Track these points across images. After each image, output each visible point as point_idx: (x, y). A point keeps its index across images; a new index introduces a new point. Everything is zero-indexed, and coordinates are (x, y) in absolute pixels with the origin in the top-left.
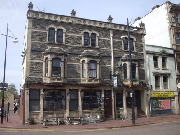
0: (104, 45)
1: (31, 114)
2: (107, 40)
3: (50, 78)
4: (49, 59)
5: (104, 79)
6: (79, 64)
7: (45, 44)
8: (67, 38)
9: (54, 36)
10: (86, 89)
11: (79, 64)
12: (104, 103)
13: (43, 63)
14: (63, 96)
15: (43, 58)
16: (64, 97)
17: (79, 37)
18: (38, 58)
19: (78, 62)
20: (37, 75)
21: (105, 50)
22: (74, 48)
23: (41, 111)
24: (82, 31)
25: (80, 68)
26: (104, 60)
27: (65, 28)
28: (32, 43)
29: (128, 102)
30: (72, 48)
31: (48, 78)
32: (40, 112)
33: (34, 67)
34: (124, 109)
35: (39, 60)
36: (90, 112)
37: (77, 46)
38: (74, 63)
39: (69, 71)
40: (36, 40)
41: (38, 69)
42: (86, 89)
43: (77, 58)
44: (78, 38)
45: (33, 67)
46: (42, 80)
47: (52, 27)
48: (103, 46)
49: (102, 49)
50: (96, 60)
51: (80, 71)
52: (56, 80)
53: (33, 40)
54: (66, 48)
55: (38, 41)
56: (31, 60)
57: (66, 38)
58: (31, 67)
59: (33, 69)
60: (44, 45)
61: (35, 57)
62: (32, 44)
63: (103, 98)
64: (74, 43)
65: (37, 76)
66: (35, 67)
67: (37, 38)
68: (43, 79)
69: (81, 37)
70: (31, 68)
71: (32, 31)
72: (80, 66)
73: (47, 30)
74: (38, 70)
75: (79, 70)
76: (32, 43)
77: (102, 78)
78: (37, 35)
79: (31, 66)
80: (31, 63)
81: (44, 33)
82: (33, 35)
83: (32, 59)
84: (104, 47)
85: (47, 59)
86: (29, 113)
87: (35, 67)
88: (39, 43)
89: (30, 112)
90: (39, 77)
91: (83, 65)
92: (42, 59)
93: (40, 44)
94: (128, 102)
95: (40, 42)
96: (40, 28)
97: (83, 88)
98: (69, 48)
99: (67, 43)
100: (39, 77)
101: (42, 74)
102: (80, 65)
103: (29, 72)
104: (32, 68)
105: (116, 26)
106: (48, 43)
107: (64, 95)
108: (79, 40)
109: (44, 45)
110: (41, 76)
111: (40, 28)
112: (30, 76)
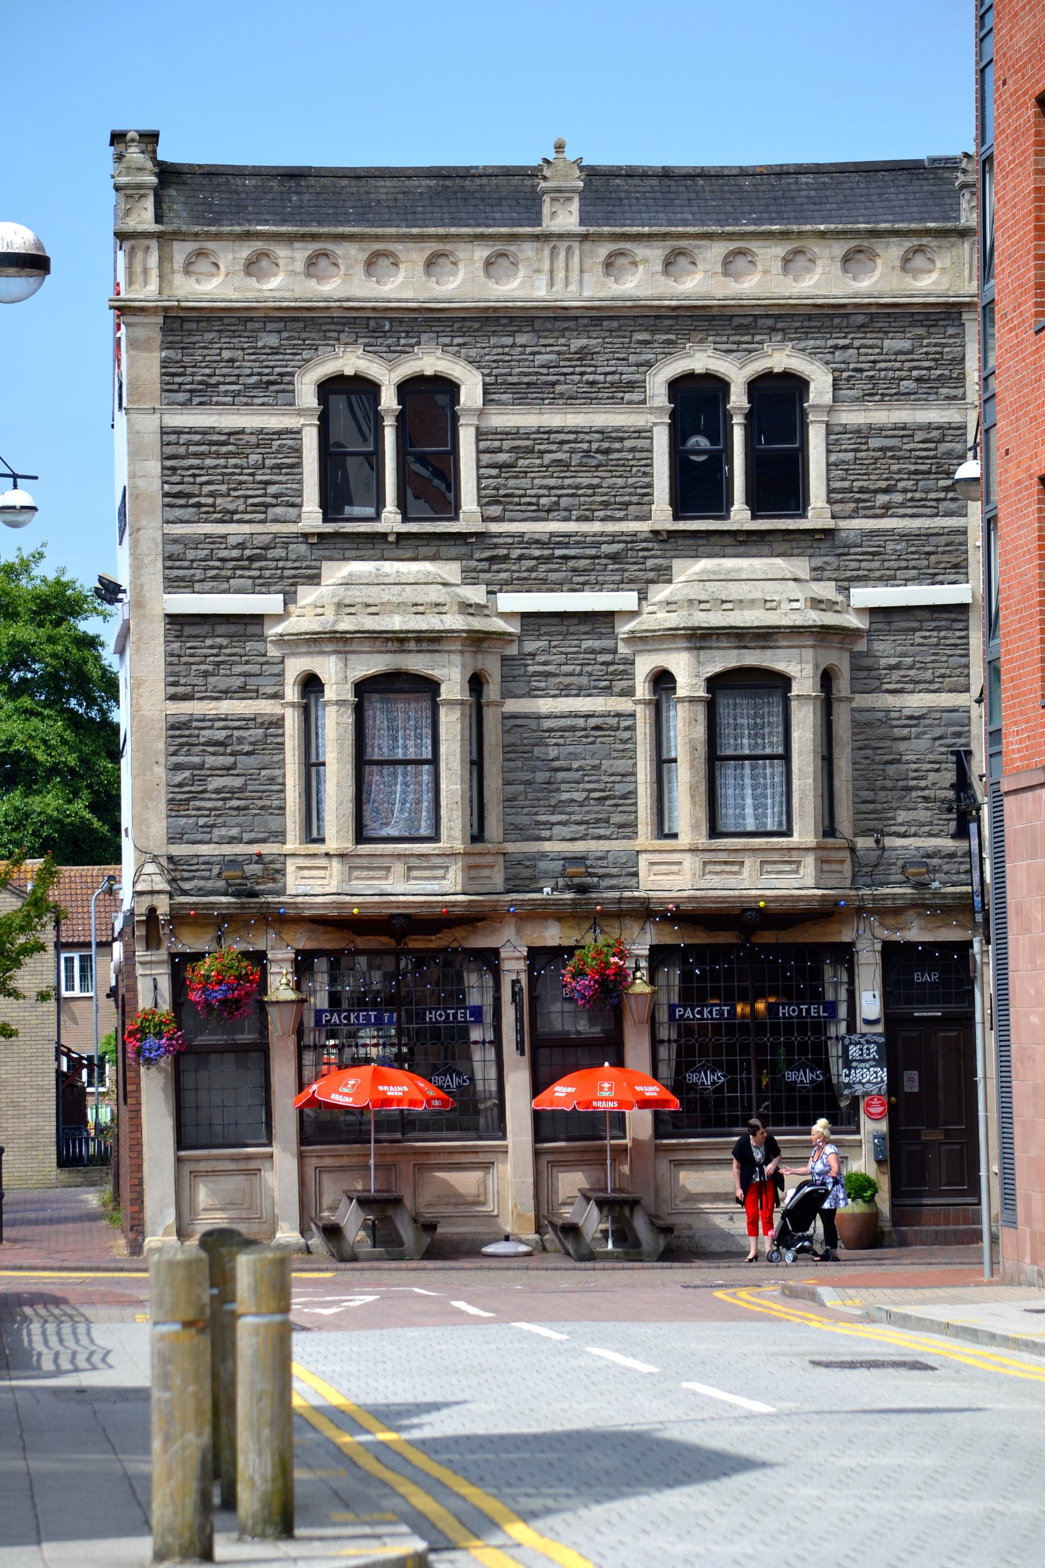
0: (886, 491)
1: (195, 1174)
2: (928, 427)
3: (342, 856)
4: (330, 693)
5: (889, 842)
6: (624, 705)
7: (287, 541)
8: (502, 457)
9: (484, 452)
10: (701, 938)
11: (624, 705)
12: (883, 1074)
13: (278, 722)
14: (831, 1008)
15: (281, 674)
16: (843, 1011)
17: (617, 435)
18: (238, 682)
19: (607, 691)
20: (234, 832)
21: (905, 536)
22: (566, 558)
23: (510, 1141)
24: (649, 364)
25: (631, 740)
26: (879, 647)
27: (474, 362)
28: (177, 549)
29: (692, 1078)
30: (549, 559)
31: (323, 862)
32: (271, 1156)
33: (201, 767)
34: (859, 1144)
35: (243, 692)
36: (253, 1165)
37: (596, 527)
38: (545, 705)
39: (528, 776)
40: (206, 513)
41: (238, 782)
42: (701, 938)
43: (603, 651)
44: (606, 452)
45: (196, 760)
46: (282, 872)
47: (349, 371)
48: (882, 499)
49: (872, 533)
50: (416, 663)
51: (634, 774)
52: (750, 863)
53: (178, 512)
54: (491, 559)
55: (228, 516)
56: (173, 698)
57: (486, 458)
58: (177, 767)
59: (192, 781)
60: (279, 552)
61: (206, 674)
62: (170, 558)
63: (868, 1022)
64: (564, 502)
65: (232, 840)
66: (210, 761)
67: (212, 494)
68: (291, 866)
69: (644, 433)
70: (179, 777)
71: (164, 431)
72: (631, 728)
73: (301, 412)
74: (242, 789)
75: (621, 765)
76: (175, 541)
77: (866, 833)
78: (209, 462)
79: (174, 754)
80: (177, 727)
81: (280, 433)
82: (174, 469)
83: (180, 690)
84: (887, 507)
85: (663, 680)
86: (179, 1160)
87: (210, 761)
88: (232, 541)
89: (539, 1146)
90: (255, 849)
91: (658, 710)
92: (270, 690)
93: (241, 546)
94: (692, 1078)
95: (246, 528)
96: (236, 394)
97: (670, 936)
98: (521, 558)
99: (495, 510)
100: (255, 849)
101: (274, 824)
102: (633, 715)
103: (163, 807)
104: (187, 774)
105: (377, 255)
106: (321, 536)
107: (843, 995)
108: (623, 463)
109: (279, 552)
110: (264, 841)
111: (236, 394)
112: (172, 840)
